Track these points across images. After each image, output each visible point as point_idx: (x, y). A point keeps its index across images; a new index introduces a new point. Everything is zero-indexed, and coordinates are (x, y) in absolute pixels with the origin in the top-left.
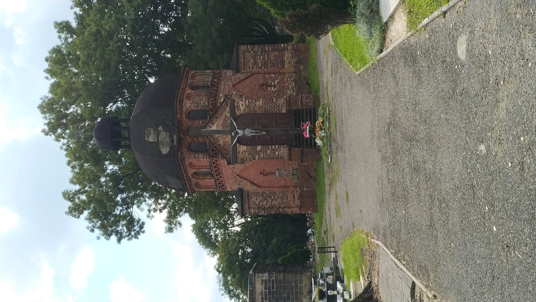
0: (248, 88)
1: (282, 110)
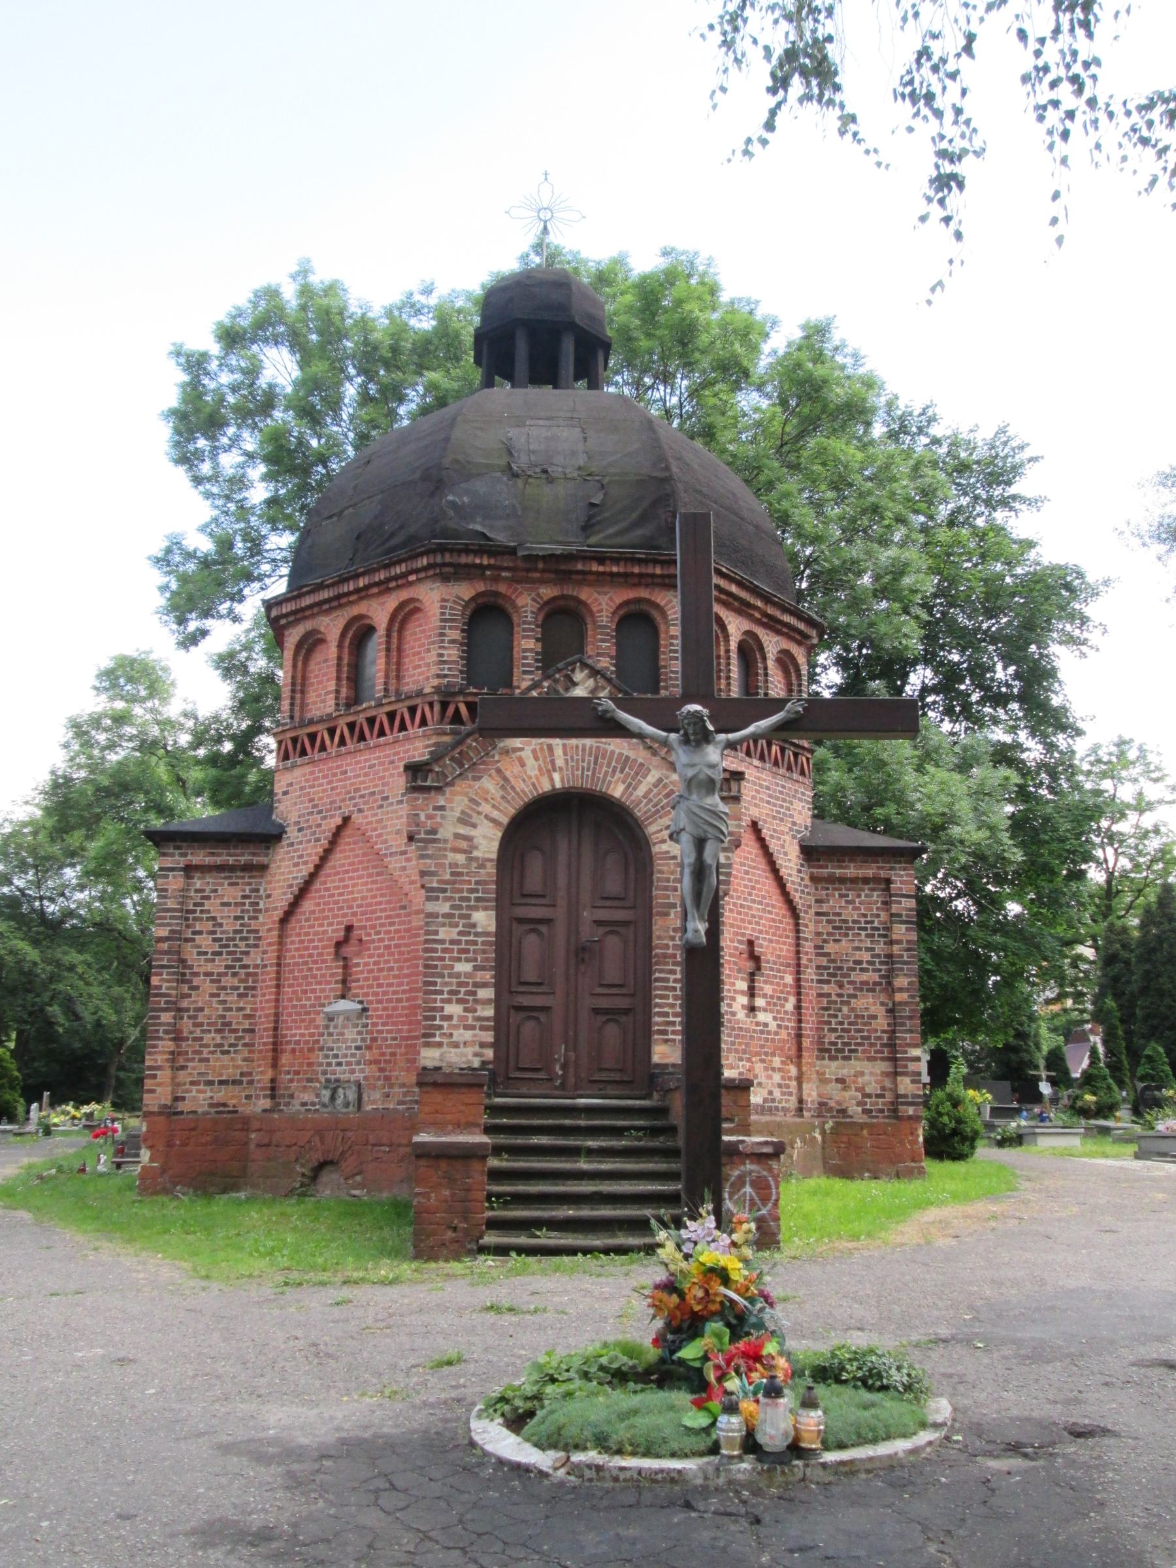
0: (746, 886)
1: (666, 1041)
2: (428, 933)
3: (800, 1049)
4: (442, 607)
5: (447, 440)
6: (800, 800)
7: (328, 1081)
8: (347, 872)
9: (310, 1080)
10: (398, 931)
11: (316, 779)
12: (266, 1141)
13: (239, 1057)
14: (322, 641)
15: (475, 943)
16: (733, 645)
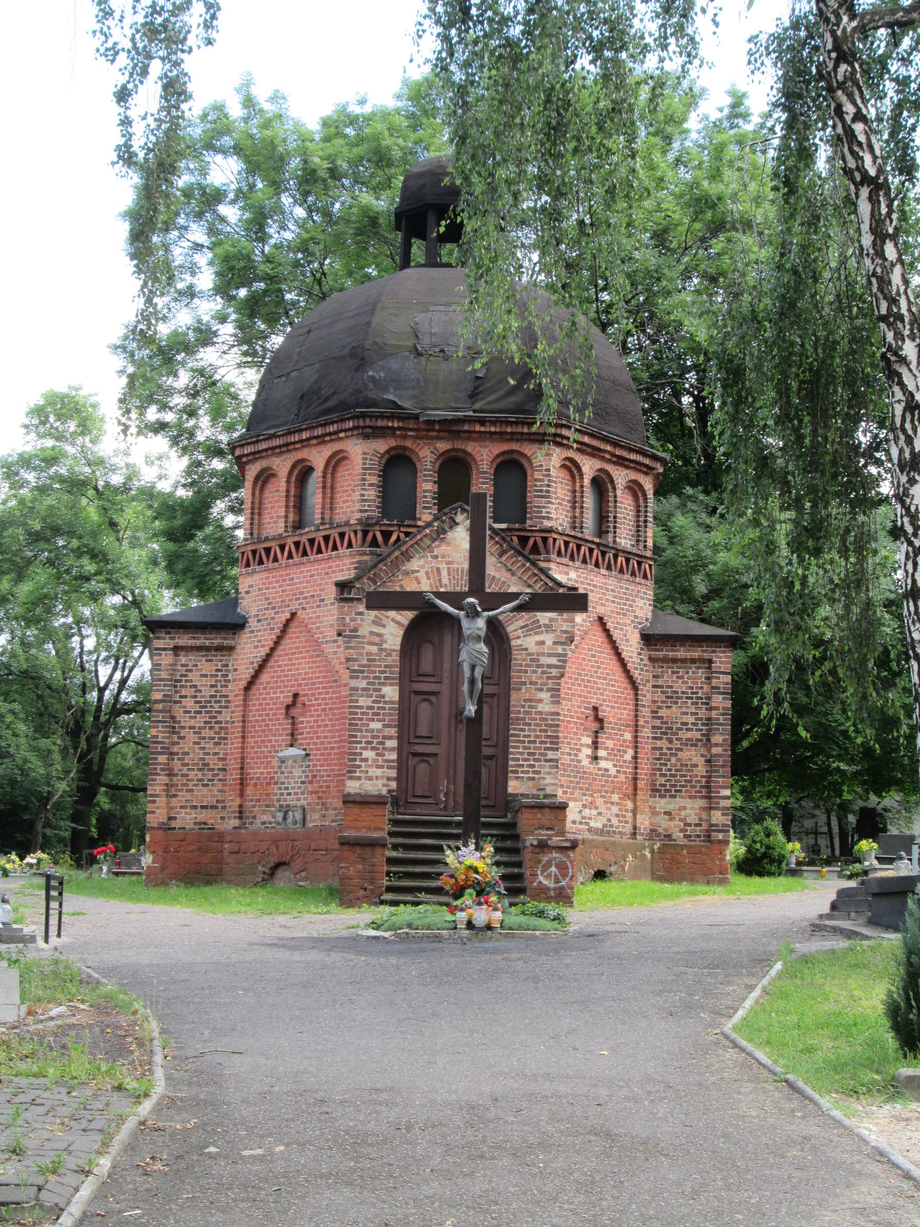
0: (592, 666)
1: (517, 778)
2: (351, 701)
3: (635, 789)
4: (364, 459)
5: (369, 324)
6: (642, 598)
7: (281, 806)
8: (294, 654)
9: (268, 806)
10: (331, 698)
11: (271, 583)
12: (236, 849)
13: (216, 789)
14: (274, 475)
15: (384, 709)
16: (587, 481)
